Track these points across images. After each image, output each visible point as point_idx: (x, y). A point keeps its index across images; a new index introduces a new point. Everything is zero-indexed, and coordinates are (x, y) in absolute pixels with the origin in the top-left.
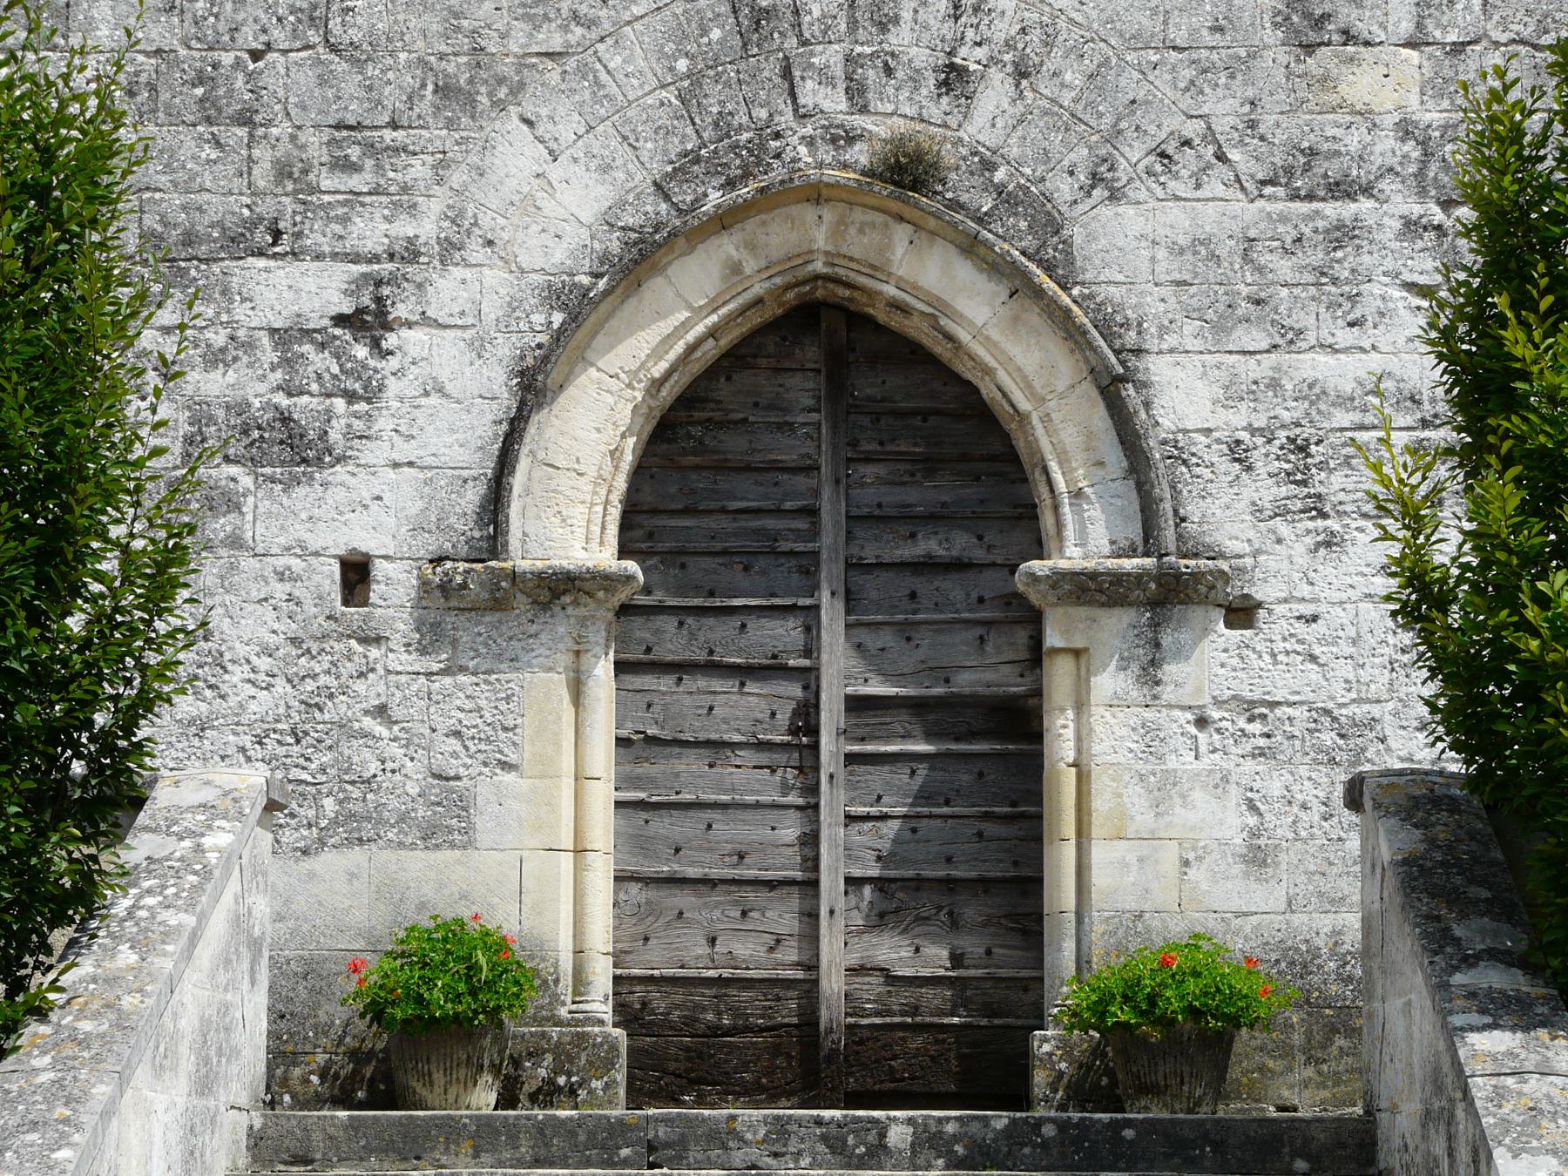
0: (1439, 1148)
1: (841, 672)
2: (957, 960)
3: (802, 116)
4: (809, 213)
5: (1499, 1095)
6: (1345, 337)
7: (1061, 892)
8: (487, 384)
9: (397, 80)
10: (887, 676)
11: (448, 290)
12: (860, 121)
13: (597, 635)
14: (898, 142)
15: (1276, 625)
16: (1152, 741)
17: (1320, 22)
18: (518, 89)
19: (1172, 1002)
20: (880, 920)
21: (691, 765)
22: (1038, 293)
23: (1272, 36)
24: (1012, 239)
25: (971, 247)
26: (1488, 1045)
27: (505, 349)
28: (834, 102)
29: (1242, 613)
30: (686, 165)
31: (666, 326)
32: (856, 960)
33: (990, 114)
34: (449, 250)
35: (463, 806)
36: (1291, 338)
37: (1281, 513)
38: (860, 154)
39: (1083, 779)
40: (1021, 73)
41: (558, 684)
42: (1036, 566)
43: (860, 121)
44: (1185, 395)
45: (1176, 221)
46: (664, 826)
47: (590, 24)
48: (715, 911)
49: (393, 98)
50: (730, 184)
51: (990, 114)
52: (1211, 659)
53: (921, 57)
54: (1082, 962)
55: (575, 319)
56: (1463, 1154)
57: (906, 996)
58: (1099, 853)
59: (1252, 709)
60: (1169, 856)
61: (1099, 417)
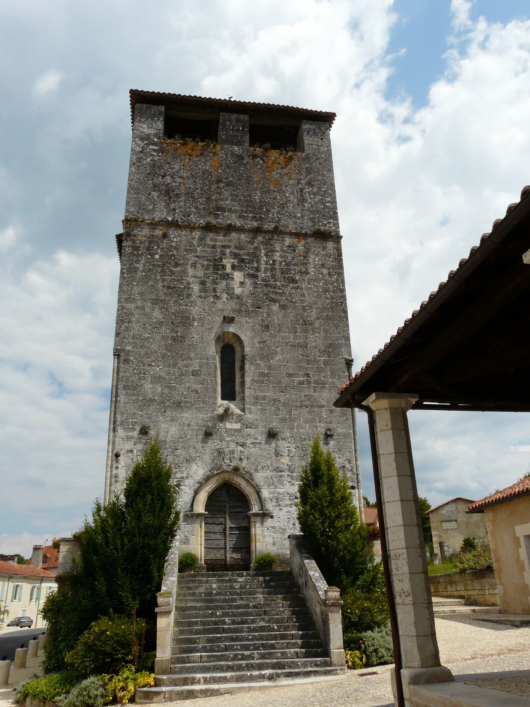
0: (301, 572)
1: (229, 524)
2: (241, 556)
3: (225, 463)
4: (226, 474)
5: (308, 566)
6: (282, 487)
7: (253, 548)
8: (191, 492)
9: (181, 459)
10: (234, 525)
11: (187, 482)
12: (231, 464)
13: (203, 520)
14: (235, 466)
15: (275, 518)
16: (262, 530)
17: (278, 454)
18: (194, 460)
19: (267, 560)
20: (233, 552)
21: (212, 535)
22: (250, 482)
23: (274, 455)
24: (247, 477)
25: (243, 477)
26: (306, 561)
27: (193, 488)
28: (228, 462)
29: (272, 517)
30: (213, 468)
31: (210, 486)
32: (231, 556)
33: (244, 463)
34: (187, 478)
35: (188, 540)
36: (276, 487)
37: (276, 506)
38: (231, 467)
39: (255, 536)
40: (248, 459)
41: (199, 525)
42: (250, 512)
43: (231, 464)
44: (265, 493)
45: (264, 475)
46: (209, 542)
47: (202, 453)
48: (215, 551)
49: (181, 461)
50: (217, 471)
51: (244, 463)
52: (269, 522)
53: (237, 457)
54: (256, 556)
55: (201, 485)
56: (304, 572)
57: (236, 561)
58: (257, 544)
59: (273, 527)
60: (265, 544)
61: (257, 496)
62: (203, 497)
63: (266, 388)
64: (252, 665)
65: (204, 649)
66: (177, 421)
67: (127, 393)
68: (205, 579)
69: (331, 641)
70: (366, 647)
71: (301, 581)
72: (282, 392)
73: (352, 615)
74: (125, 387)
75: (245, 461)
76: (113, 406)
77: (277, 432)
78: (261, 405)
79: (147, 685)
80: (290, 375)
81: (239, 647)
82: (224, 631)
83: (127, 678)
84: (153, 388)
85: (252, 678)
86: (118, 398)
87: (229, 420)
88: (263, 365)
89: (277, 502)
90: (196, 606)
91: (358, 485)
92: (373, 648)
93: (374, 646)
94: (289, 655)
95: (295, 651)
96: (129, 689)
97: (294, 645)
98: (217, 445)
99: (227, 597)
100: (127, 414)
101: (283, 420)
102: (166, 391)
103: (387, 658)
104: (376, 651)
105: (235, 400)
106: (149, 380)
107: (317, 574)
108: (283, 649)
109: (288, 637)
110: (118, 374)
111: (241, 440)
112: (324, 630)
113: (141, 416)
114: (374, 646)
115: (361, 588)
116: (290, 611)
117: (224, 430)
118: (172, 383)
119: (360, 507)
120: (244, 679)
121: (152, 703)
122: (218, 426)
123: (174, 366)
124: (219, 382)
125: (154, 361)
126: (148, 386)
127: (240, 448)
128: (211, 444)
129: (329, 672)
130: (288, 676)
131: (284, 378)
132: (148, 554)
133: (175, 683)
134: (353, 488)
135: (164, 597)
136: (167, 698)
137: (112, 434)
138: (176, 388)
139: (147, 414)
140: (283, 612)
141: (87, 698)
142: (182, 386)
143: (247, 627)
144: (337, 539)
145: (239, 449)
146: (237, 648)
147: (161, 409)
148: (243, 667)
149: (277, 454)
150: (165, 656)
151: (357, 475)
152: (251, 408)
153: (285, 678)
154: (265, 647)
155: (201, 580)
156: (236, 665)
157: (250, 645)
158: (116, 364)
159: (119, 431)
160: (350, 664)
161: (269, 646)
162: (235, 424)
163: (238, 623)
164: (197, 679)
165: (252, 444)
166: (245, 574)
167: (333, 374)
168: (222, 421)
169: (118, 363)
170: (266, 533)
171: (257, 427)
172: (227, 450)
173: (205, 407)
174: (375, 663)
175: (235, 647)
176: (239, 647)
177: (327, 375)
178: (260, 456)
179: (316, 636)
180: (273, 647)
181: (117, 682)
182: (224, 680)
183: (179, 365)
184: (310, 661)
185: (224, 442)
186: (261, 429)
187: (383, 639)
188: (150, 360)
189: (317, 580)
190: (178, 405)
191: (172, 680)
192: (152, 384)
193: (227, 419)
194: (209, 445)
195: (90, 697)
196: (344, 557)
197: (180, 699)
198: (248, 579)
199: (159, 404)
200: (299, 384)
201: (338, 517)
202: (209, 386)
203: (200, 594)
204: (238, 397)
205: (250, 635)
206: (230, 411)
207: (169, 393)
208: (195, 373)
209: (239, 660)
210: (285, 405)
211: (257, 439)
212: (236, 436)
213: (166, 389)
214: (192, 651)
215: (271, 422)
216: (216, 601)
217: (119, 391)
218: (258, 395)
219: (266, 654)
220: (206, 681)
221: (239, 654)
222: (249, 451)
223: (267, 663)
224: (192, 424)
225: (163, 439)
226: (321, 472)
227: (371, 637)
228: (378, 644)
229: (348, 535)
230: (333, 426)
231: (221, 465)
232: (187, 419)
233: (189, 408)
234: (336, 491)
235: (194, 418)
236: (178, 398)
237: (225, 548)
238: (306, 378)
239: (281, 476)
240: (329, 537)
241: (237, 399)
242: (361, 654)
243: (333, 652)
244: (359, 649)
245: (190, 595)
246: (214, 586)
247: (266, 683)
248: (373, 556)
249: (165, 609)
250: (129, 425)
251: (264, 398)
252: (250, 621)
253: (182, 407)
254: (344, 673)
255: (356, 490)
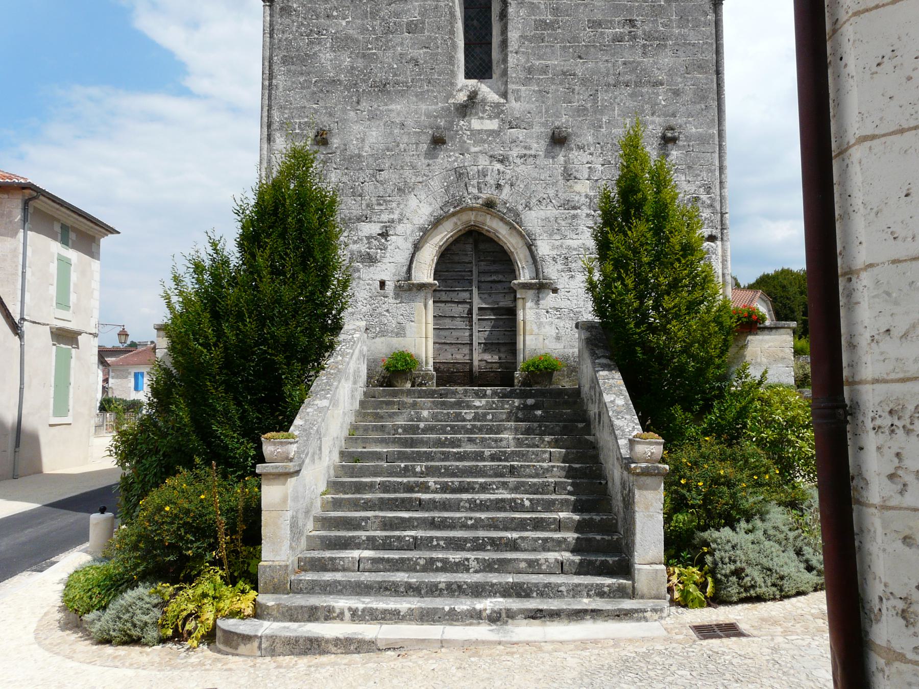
1: (477, 303)
2: (500, 358)
3: (469, 194)
4: (470, 213)
5: (605, 383)
6: (575, 237)
7: (520, 345)
8: (408, 247)
11: (400, 228)
13: (429, 295)
15: (562, 293)
20: (485, 351)
21: (448, 321)
22: (515, 228)
23: (560, 178)
24: (510, 218)
25: (502, 219)
26: (603, 373)
27: (411, 240)
28: (475, 191)
29: (555, 291)
30: (446, 204)
31: (442, 235)
32: (480, 359)
34: (400, 221)
35: (404, 329)
36: (565, 237)
38: (480, 201)
40: (512, 185)
41: (422, 305)
42: (515, 281)
44: (544, 248)
45: (542, 214)
46: (443, 333)
50: (455, 207)
52: (550, 300)
53: (492, 182)
55: (425, 234)
57: (490, 366)
58: (527, 338)
59: (557, 309)
62: (429, 256)
63: (548, 50)
64: (459, 587)
65: (372, 543)
66: (381, 119)
67: (289, 71)
68: (410, 400)
69: (638, 546)
70: (715, 563)
71: (593, 410)
72: (580, 57)
73: (689, 491)
74: (285, 61)
75: (506, 190)
76: (266, 97)
77: (569, 135)
78: (538, 84)
79: (234, 614)
80: (595, 24)
81: (442, 543)
82: (421, 505)
83: (204, 595)
84: (335, 59)
85: (452, 617)
86: (274, 81)
87: (477, 114)
88: (542, 7)
89: (566, 264)
90: (380, 453)
91: (722, 234)
92: (733, 567)
93: (735, 562)
94: (544, 567)
95: (556, 560)
96: (203, 618)
97: (559, 545)
98: (455, 161)
99: (443, 437)
100: (290, 109)
101: (581, 111)
102: (360, 63)
103: (764, 589)
104: (738, 573)
105: (491, 78)
106: (328, 45)
107: (620, 402)
108: (534, 550)
109: (549, 524)
110: (271, 37)
111: (499, 151)
112: (625, 519)
113: (316, 111)
114: (735, 562)
115: (715, 430)
116: (563, 468)
117: (468, 133)
118: (370, 49)
119: (723, 274)
120: (436, 617)
121: (237, 655)
122: (457, 125)
123: (374, 15)
124: (461, 44)
125: (336, 9)
126: (326, 57)
127: (498, 166)
128: (443, 159)
129: (626, 615)
130: (533, 618)
131: (585, 30)
132: (271, 355)
133: (292, 615)
134: (712, 238)
135: (274, 444)
136: (265, 649)
137: (265, 146)
138: (378, 58)
139: (326, 108)
140: (548, 470)
141: (129, 625)
142: (389, 53)
143: (468, 501)
144: (667, 332)
145: (496, 168)
146: (438, 544)
147: (351, 97)
148: (441, 590)
149: (568, 176)
150: (278, 558)
151: (722, 214)
152: (518, 90)
153: (526, 621)
154: (497, 545)
155: (403, 402)
156: (427, 584)
157: (466, 540)
158: (268, 18)
159: (278, 141)
160: (677, 595)
161: (506, 544)
162: (488, 121)
163: (454, 491)
164: (338, 611)
165: (521, 157)
166: (489, 392)
167: (683, 19)
168: (464, 117)
169: (271, 16)
170: (544, 320)
171: (530, 125)
172: (473, 170)
173: (433, 91)
174: (735, 599)
175: (435, 543)
176: (442, 543)
177: (670, 20)
178: (535, 179)
179: (609, 527)
180: (513, 546)
181: (183, 601)
182: (394, 616)
183: (382, 14)
184: (586, 586)
185: (467, 156)
186: (537, 129)
187: (756, 547)
188: (328, 6)
189: (618, 413)
190: (382, 88)
191: (285, 610)
192: (334, 51)
193: (474, 111)
194: (439, 160)
195: (135, 626)
196: (682, 369)
197: (293, 654)
198: (493, 402)
199: (347, 88)
200: (614, 40)
201: (674, 285)
202: (440, 51)
203: (395, 428)
204: (496, 71)
205: (471, 519)
206: (479, 97)
207: (366, 67)
208: (412, 28)
209: (438, 570)
210: (584, 82)
211: (530, 149)
212: (490, 143)
213: (360, 60)
214: (346, 544)
215: (557, 115)
216: (422, 443)
217: (275, 68)
218: (533, 65)
219: (495, 561)
220: (356, 616)
221: (438, 560)
222: (514, 171)
223: (493, 585)
224: (409, 122)
225: (356, 152)
226: (640, 195)
227: (729, 541)
228: (743, 558)
229: (692, 322)
230: (680, 120)
231: (462, 197)
232: (398, 114)
233: (402, 94)
234: (671, 232)
235: (412, 112)
236: (381, 76)
237: (471, 344)
238: (627, 29)
239: (574, 217)
240: (653, 329)
241: (494, 76)
242: (704, 576)
243: (639, 570)
244: (700, 563)
245: (375, 429)
246: (425, 413)
247: (482, 631)
248: (745, 368)
249: (277, 467)
250: (295, 129)
251: (544, 70)
252: (477, 486)
253: (389, 92)
254: (661, 618)
255: (719, 243)
